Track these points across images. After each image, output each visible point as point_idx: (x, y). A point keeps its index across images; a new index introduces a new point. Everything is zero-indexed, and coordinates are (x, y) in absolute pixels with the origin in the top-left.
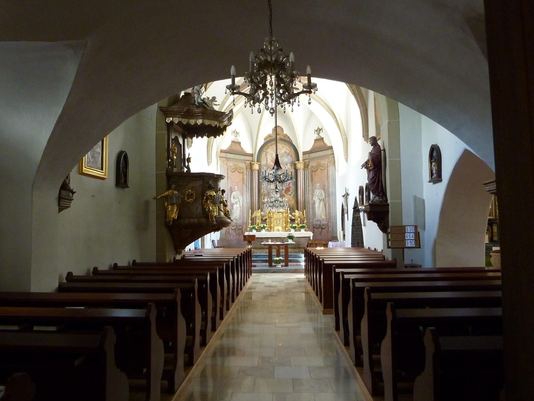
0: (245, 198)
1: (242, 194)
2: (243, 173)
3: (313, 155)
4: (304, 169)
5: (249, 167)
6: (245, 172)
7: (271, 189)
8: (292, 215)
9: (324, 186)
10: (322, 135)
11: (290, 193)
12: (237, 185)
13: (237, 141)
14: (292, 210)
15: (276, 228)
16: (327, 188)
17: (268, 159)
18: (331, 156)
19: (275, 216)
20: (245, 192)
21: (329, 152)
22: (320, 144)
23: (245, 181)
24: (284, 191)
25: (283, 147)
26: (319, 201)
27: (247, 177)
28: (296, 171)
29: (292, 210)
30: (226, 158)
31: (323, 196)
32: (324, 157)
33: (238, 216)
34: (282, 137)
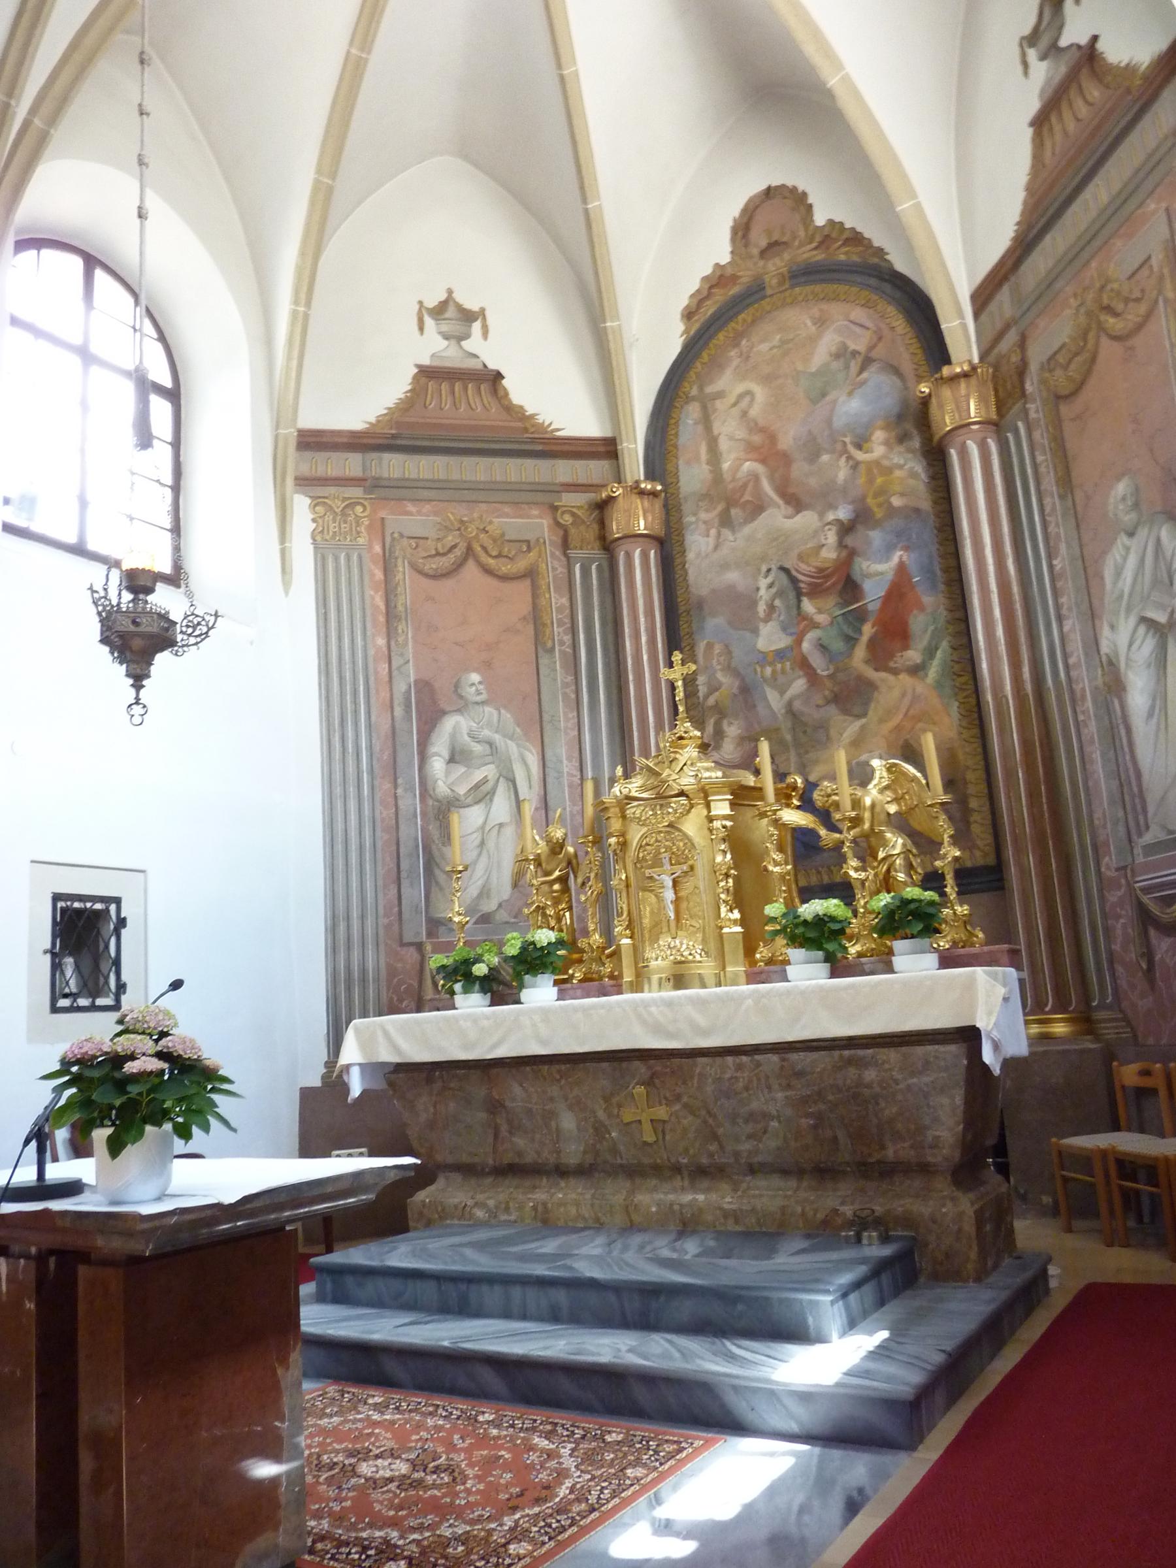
1: (537, 727)
2: (530, 574)
6: (552, 566)
7: (764, 659)
11: (913, 655)
12: (486, 667)
13: (471, 364)
15: (658, 961)
17: (724, 445)
20: (560, 712)
23: (559, 633)
24: (860, 652)
26: (1147, 646)
30: (373, 485)
34: (808, 254)
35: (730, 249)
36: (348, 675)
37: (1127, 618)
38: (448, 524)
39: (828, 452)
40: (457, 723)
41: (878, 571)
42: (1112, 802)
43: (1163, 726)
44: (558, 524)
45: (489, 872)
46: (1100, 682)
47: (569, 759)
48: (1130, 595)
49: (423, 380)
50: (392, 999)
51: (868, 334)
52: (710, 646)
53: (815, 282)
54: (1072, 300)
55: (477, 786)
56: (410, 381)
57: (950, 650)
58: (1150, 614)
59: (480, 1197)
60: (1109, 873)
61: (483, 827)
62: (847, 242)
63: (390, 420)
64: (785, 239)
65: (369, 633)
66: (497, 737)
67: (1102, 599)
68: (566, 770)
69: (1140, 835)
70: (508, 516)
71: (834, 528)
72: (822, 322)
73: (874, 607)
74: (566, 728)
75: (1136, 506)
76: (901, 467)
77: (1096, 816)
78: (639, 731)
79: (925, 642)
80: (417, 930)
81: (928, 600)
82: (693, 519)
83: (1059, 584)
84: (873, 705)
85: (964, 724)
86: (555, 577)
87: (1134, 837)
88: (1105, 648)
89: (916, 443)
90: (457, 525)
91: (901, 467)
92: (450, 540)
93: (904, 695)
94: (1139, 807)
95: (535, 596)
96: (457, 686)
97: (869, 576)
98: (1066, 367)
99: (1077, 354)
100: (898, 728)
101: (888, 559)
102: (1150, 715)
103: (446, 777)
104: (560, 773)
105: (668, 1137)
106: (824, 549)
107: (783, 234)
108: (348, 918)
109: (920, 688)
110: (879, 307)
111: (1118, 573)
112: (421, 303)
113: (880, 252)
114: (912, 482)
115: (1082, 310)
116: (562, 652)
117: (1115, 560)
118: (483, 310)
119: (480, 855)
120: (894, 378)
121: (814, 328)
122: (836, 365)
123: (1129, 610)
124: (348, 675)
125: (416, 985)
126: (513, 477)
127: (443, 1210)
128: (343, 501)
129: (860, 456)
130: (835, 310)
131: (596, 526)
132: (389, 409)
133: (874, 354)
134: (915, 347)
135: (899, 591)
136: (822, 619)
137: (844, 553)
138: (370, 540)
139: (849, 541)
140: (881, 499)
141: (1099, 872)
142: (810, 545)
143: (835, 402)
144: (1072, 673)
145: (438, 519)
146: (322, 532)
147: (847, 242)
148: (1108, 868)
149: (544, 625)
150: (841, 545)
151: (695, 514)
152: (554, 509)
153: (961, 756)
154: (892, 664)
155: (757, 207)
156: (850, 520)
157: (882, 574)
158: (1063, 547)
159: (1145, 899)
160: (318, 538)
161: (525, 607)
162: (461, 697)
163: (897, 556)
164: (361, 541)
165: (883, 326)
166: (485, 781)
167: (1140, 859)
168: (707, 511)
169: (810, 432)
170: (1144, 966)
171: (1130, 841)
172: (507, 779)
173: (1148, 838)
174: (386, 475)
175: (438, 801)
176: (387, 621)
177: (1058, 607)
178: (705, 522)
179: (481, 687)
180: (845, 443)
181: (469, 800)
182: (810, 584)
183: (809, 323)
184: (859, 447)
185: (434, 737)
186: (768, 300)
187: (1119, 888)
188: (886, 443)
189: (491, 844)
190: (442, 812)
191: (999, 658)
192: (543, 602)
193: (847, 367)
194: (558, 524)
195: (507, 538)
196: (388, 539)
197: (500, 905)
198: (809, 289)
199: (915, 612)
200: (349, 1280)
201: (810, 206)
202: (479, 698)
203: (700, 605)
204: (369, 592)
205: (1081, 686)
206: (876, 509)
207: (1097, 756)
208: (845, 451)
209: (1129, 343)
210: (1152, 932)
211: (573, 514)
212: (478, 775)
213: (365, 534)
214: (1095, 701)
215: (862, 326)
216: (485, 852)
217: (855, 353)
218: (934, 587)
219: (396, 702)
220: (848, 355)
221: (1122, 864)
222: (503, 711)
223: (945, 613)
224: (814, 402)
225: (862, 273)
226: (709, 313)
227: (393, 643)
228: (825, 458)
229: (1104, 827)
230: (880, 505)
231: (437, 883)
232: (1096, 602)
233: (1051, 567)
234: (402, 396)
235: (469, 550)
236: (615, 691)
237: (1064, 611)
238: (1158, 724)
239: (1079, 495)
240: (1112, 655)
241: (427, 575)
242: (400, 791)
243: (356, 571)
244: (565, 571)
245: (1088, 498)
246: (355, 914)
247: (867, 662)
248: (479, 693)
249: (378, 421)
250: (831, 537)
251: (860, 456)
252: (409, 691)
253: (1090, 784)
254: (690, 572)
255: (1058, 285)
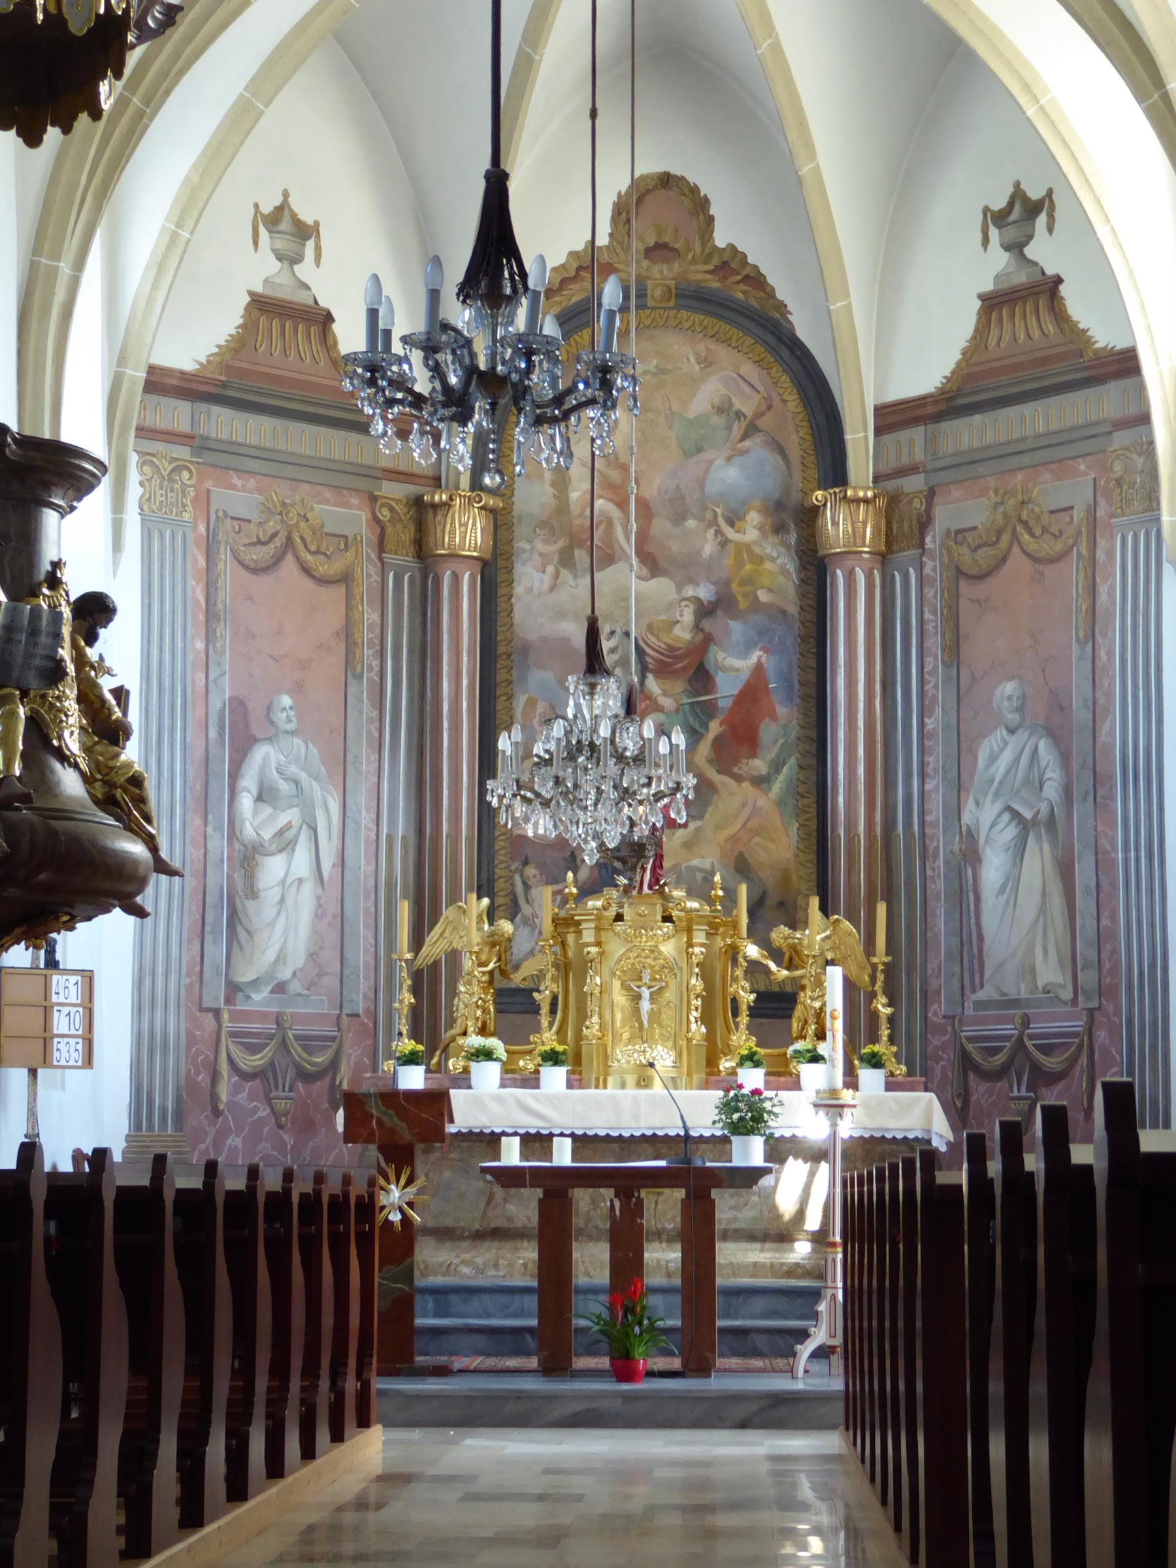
0: (361, 799)
1: (340, 767)
2: (345, 579)
3: (966, 434)
4: (884, 557)
5: (407, 534)
6: (367, 574)
8: (765, 944)
9: (1059, 705)
10: (1046, 252)
11: (759, 765)
12: (298, 689)
13: (301, 297)
14: (773, 909)
15: (625, 1056)
16: (1080, 714)
18: (1121, 438)
19: (616, 948)
20: (363, 755)
21: (1106, 401)
22: (1027, 332)
23: (368, 654)
25: (707, 363)
26: (1008, 833)
27: (380, 617)
28: (815, 569)
29: (773, 909)
30: (199, 444)
31: (1052, 791)
32: (1056, 449)
33: (298, 958)
34: (700, 275)
35: (609, 230)
36: (167, 684)
37: (993, 802)
38: (271, 506)
39: (695, 518)
40: (268, 754)
41: (735, 665)
42: (949, 955)
43: (1012, 904)
44: (376, 519)
45: (285, 934)
46: (956, 847)
47: (368, 811)
48: (1001, 783)
49: (255, 313)
50: (189, 1070)
51: (757, 397)
52: (531, 703)
53: (706, 313)
54: (992, 493)
55: (280, 833)
56: (242, 312)
57: (796, 768)
58: (1017, 806)
59: (467, 1256)
60: (935, 1019)
61: (283, 882)
62: (746, 279)
63: (220, 363)
64: (677, 246)
65: (189, 633)
66: (303, 776)
67: (972, 775)
68: (363, 822)
69: (974, 991)
70: (327, 502)
71: (692, 606)
72: (707, 363)
73: (725, 704)
74: (367, 772)
75: (1020, 709)
76: (773, 560)
77: (930, 966)
78: (449, 789)
79: (773, 754)
80: (215, 995)
81: (781, 710)
82: (527, 546)
83: (927, 743)
84: (710, 809)
85: (802, 847)
86: (369, 585)
87: (967, 991)
88: (966, 818)
89: (792, 538)
90: (279, 508)
91: (773, 560)
92: (272, 525)
93: (744, 805)
94: (976, 967)
95: (349, 608)
96: (269, 709)
97: (724, 669)
98: (975, 550)
99: (986, 544)
100: (734, 839)
101: (746, 655)
102: (1002, 890)
103: (254, 817)
104: (358, 824)
105: (660, 1206)
106: (678, 627)
107: (676, 239)
108: (154, 973)
109: (762, 802)
110: (774, 371)
111: (993, 759)
112: (256, 206)
113: (782, 307)
114: (781, 578)
115: (1001, 509)
116: (370, 680)
117: (991, 747)
118: (317, 224)
119: (278, 914)
120: (780, 459)
121: (697, 368)
122: (718, 420)
123: (997, 795)
124: (167, 684)
125: (212, 1057)
126: (337, 455)
127: (426, 1267)
128: (170, 463)
129: (730, 533)
130: (724, 353)
131: (412, 528)
132: (218, 346)
133: (761, 423)
134: (805, 431)
135: (753, 693)
136: (667, 702)
137: (700, 636)
138: (195, 518)
139: (707, 624)
140: (748, 589)
141: (925, 1017)
142: (663, 617)
143: (711, 462)
144: (927, 830)
145: (262, 498)
146: (149, 500)
147: (746, 279)
148: (935, 1014)
149: (355, 644)
150: (697, 627)
151: (530, 541)
152: (373, 499)
153: (794, 877)
154: (735, 770)
155: (648, 191)
156: (710, 602)
157: (737, 670)
158: (938, 711)
159: (969, 1047)
160: (145, 507)
161: (338, 622)
162: (272, 723)
163: (756, 655)
164: (187, 516)
165: (775, 395)
166: (289, 826)
167: (970, 1010)
168: (545, 541)
169: (678, 487)
170: (959, 1105)
171: (963, 995)
172: (310, 827)
173: (981, 995)
174: (213, 435)
175: (244, 845)
176: (207, 620)
177: (922, 765)
178: (541, 555)
179: (292, 713)
180: (715, 512)
181: (273, 848)
182: (659, 661)
183: (693, 360)
184: (732, 524)
185: (245, 767)
186: (648, 311)
187: (945, 1033)
188: (761, 528)
189: (290, 901)
190: (248, 859)
191: (857, 797)
192: (356, 616)
193: (729, 428)
194: (376, 519)
195: (326, 530)
196: (213, 518)
197: (294, 974)
198: (698, 317)
199: (767, 720)
200: (453, 1298)
201: (711, 219)
202: (289, 727)
203: (525, 650)
204: (191, 582)
205: (935, 844)
206: (740, 598)
207: (941, 912)
208: (714, 522)
209: (1041, 568)
210: (971, 1076)
211: (392, 509)
212: (284, 818)
213: (190, 508)
214: (947, 863)
215: (750, 384)
216: (284, 909)
217: (739, 414)
218: (789, 698)
219: (211, 723)
220: (732, 415)
221: (951, 1013)
222: (310, 745)
223: (797, 728)
224: (687, 454)
225: (758, 323)
226: (574, 300)
227: (211, 648)
228: (691, 523)
229: (938, 977)
230: (745, 595)
231: (239, 942)
232: (964, 776)
233: (922, 725)
234: (234, 332)
235: (289, 539)
236: (415, 735)
237: (929, 770)
238: (1007, 901)
239: (965, 673)
240: (972, 827)
241: (246, 567)
242: (209, 829)
243: (180, 554)
244: (379, 579)
245: (974, 680)
246: (160, 970)
247: (710, 761)
248: (289, 721)
249: (209, 362)
250: (687, 615)
251: (730, 533)
252: (223, 710)
253: (929, 935)
254: (517, 608)
255: (981, 469)
